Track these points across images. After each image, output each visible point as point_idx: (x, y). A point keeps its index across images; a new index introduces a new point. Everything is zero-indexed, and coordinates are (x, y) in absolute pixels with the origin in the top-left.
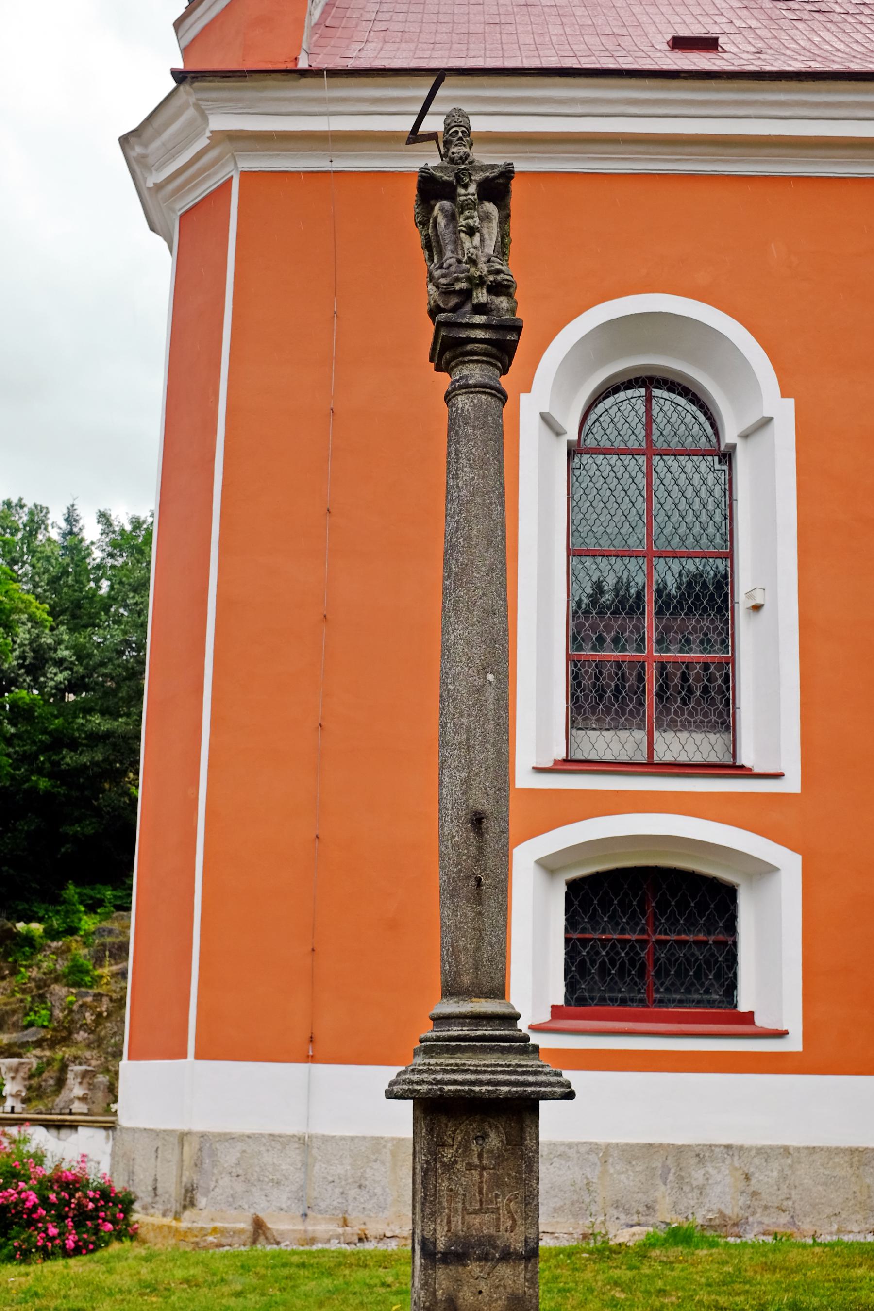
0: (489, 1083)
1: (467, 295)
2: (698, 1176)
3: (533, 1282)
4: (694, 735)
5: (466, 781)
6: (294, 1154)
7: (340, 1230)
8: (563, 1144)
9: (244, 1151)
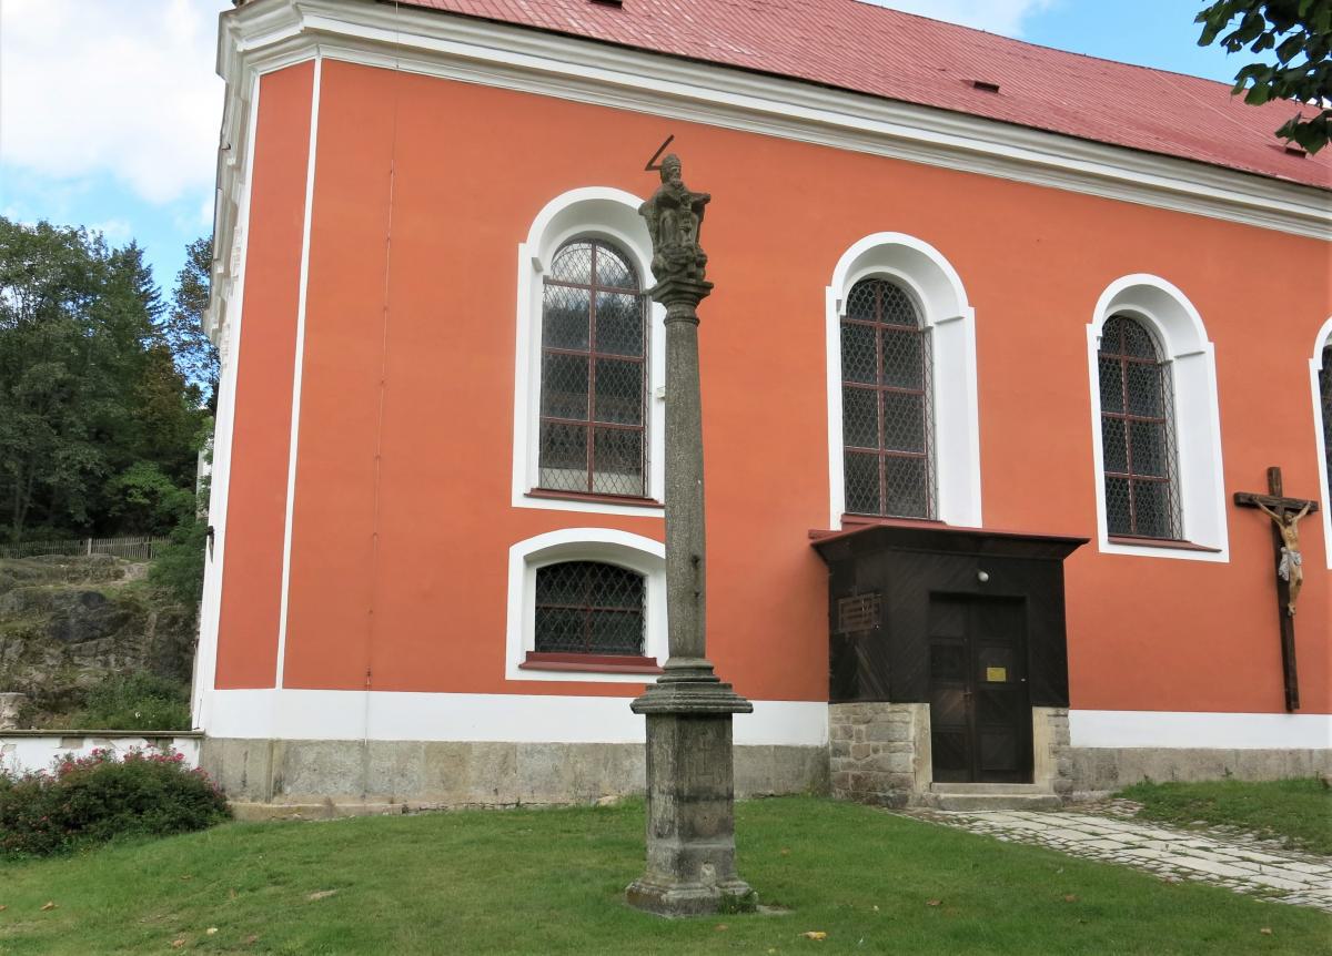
0: (714, 704)
1: (685, 266)
2: (627, 763)
3: (731, 811)
4: (603, 474)
5: (689, 539)
6: (356, 754)
7: (389, 806)
8: (540, 744)
9: (319, 753)
